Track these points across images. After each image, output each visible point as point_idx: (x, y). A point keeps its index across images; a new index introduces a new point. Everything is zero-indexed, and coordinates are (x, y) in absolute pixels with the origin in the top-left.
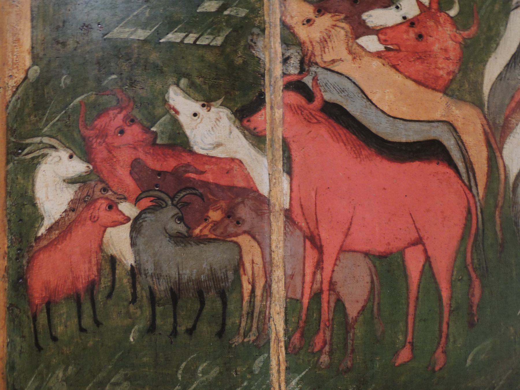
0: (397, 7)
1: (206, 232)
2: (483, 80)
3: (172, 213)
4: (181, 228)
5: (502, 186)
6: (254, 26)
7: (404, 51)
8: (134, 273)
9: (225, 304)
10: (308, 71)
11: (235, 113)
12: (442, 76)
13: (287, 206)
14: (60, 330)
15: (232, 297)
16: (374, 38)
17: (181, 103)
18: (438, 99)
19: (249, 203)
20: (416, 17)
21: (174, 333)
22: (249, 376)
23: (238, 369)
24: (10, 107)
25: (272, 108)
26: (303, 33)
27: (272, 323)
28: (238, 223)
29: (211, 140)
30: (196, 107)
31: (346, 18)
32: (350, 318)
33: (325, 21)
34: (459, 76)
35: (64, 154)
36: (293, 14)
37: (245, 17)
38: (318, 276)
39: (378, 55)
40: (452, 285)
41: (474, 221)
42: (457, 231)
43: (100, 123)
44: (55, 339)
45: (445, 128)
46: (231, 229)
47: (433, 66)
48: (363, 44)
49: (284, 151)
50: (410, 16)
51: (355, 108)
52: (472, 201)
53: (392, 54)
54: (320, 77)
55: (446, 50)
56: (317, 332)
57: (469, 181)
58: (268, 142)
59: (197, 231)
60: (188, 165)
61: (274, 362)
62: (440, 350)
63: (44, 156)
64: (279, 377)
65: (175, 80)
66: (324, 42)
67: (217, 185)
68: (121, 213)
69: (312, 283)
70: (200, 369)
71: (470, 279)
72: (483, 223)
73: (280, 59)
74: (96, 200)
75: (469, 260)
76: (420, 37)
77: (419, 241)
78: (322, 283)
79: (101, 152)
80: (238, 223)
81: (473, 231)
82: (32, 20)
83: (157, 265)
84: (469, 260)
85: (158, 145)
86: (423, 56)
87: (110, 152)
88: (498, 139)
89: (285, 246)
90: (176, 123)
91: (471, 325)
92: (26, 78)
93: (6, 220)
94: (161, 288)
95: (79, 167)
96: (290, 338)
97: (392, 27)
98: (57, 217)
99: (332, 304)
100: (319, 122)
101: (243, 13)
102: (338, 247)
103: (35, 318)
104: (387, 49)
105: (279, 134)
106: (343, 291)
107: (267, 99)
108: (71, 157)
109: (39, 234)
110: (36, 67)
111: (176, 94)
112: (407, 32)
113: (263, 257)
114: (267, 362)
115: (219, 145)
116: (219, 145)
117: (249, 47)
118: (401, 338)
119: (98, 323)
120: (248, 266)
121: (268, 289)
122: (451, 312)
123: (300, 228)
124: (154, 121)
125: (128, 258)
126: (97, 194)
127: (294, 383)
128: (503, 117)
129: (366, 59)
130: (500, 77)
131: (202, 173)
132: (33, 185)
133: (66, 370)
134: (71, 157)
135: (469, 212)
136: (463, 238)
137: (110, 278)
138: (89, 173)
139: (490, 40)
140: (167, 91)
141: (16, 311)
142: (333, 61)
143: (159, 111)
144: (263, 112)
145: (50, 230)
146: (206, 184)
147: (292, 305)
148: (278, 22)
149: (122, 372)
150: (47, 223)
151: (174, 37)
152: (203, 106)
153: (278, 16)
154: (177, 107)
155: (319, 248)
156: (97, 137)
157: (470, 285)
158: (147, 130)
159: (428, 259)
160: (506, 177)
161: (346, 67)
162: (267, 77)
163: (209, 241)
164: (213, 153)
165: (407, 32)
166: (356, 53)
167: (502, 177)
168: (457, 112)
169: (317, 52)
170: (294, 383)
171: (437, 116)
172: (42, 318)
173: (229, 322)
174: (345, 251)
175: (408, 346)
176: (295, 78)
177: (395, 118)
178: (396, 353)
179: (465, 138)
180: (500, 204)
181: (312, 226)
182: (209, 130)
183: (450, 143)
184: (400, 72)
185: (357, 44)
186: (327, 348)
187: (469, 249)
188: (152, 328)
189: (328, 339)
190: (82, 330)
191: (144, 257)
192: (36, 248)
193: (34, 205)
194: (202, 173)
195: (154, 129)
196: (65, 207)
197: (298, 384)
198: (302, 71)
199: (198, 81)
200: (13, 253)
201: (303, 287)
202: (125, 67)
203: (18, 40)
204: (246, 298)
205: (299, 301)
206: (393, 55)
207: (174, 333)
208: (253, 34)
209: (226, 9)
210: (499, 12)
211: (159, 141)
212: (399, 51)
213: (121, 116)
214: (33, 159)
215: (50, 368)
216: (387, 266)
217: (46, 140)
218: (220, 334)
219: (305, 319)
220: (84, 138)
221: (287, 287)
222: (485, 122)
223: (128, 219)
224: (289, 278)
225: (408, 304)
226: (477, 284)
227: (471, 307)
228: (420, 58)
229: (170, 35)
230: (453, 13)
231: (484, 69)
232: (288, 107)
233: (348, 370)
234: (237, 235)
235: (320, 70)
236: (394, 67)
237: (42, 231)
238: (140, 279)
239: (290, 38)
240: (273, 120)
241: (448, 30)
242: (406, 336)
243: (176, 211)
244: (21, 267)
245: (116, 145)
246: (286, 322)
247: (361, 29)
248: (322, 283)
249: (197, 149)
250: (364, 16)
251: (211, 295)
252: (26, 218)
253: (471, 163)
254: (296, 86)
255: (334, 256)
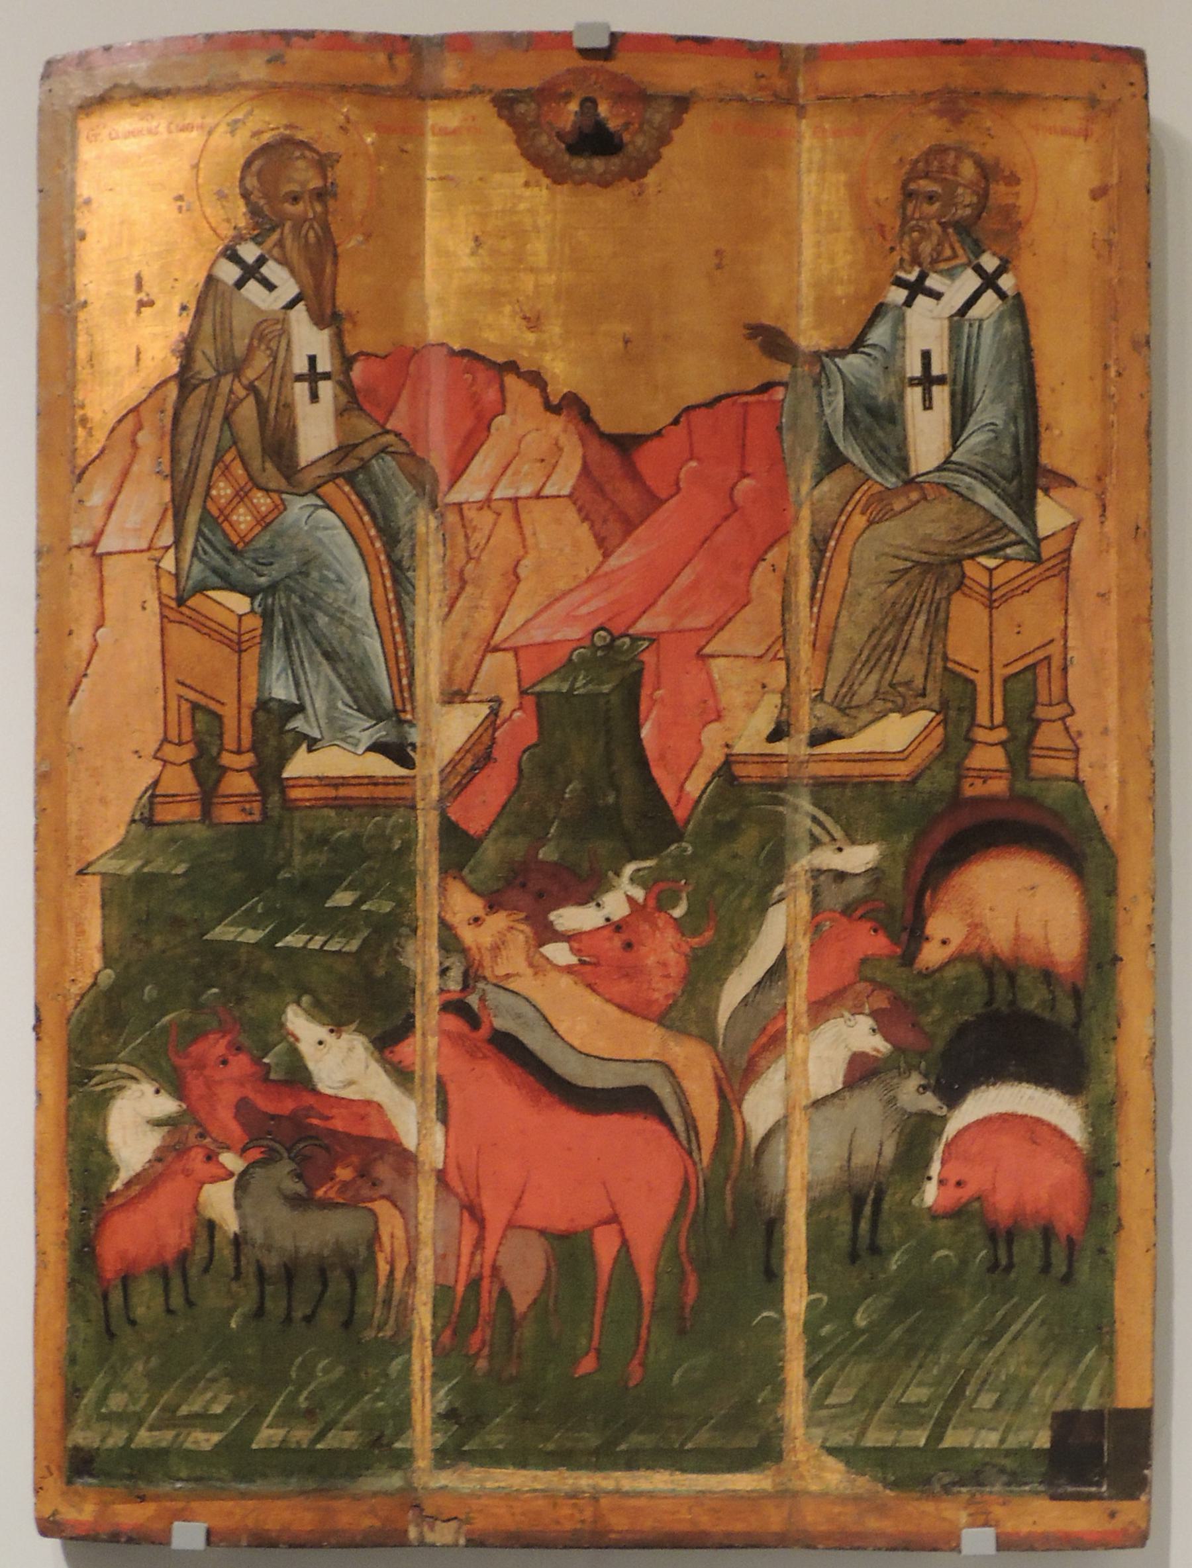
0: (598, 905)
1: (332, 1194)
2: (717, 1006)
3: (288, 1169)
4: (300, 1188)
5: (738, 1151)
6: (403, 925)
7: (606, 966)
8: (238, 1242)
9: (354, 1287)
10: (474, 988)
11: (373, 1042)
12: (657, 1000)
13: (440, 1166)
14: (140, 1312)
15: (364, 1281)
16: (564, 946)
17: (303, 1027)
18: (649, 1032)
19: (390, 1159)
20: (624, 919)
21: (288, 1319)
22: (383, 1381)
23: (370, 1370)
24: (73, 1020)
25: (424, 1035)
26: (468, 935)
27: (415, 1316)
28: (374, 1184)
29: (340, 1076)
30: (322, 1032)
31: (527, 918)
32: (517, 1312)
33: (498, 921)
34: (682, 1000)
35: (148, 1088)
36: (457, 909)
37: (390, 914)
38: (478, 1258)
39: (569, 969)
40: (657, 1279)
41: (693, 1197)
42: (668, 1208)
43: (195, 1050)
44: (133, 1323)
45: (658, 1070)
46: (366, 1192)
47: (645, 986)
48: (548, 955)
49: (438, 1092)
50: (616, 918)
51: (535, 1040)
52: (691, 1170)
53: (588, 968)
54: (489, 996)
55: (664, 964)
56: (474, 1330)
57: (689, 1142)
58: (417, 1080)
59: (320, 1193)
60: (311, 1107)
61: (416, 1367)
62: (636, 1362)
63: (121, 1088)
64: (423, 1386)
65: (294, 996)
66: (496, 949)
67: (348, 1135)
68: (223, 1167)
69: (470, 1266)
70: (320, 1366)
71: (683, 1273)
72: (707, 1198)
73: (436, 969)
74: (190, 1149)
75: (682, 1248)
76: (628, 946)
77: (614, 1219)
78: (482, 1266)
79: (196, 1086)
80: (374, 1184)
81: (692, 1209)
82: (103, 907)
83: (267, 1232)
84: (682, 1248)
85: (273, 1081)
86: (631, 972)
87: (209, 1088)
88: (736, 1087)
89: (436, 1218)
90: (294, 1053)
91: (682, 1332)
92: (95, 984)
93: (67, 1169)
94: (272, 1262)
95: (167, 1105)
96: (438, 1337)
97: (590, 932)
98: (138, 1168)
99: (495, 1295)
100: (485, 1057)
101: (387, 907)
102: (505, 1222)
103: (105, 1297)
104: (582, 963)
105: (433, 1070)
106: (509, 1279)
107: (418, 1024)
108: (157, 1092)
109: (114, 1189)
110: (109, 971)
111: (296, 1015)
112: (610, 939)
113: (407, 1231)
114: (408, 1365)
115: (351, 1083)
116: (351, 1083)
117: (395, 953)
118: (584, 1341)
119: (190, 1303)
120: (385, 1239)
121: (411, 1270)
122: (653, 1313)
123: (457, 1195)
124: (266, 1049)
125: (231, 1223)
126: (192, 1140)
127: (442, 1393)
128: (746, 1057)
129: (554, 974)
130: (745, 1001)
131: (328, 1118)
132: (105, 1125)
133: (147, 1362)
134: (157, 1092)
135: (686, 1184)
136: (676, 1218)
137: (207, 1248)
138: (182, 1114)
139: (731, 951)
140: (284, 1012)
141: (80, 1288)
142: (508, 976)
143: (273, 1037)
144: (411, 1040)
145: (128, 1185)
146: (333, 1133)
147: (442, 1294)
148: (436, 919)
149: (221, 1366)
150: (124, 1176)
151: (293, 940)
152: (332, 1031)
153: (436, 911)
154: (298, 1032)
155: (480, 1222)
156: (193, 1068)
157: (682, 1279)
158: (257, 1061)
159: (625, 1243)
160: (746, 1140)
161: (525, 984)
162: (418, 994)
163: (337, 1205)
164: (344, 1093)
165: (610, 939)
166: (539, 966)
167: (740, 1139)
168: (677, 1049)
169: (487, 962)
170: (442, 1393)
171: (648, 1053)
172: (116, 1298)
173: (359, 1310)
174: (514, 1227)
175: (592, 1354)
176: (455, 996)
177: (588, 1055)
178: (576, 1362)
179: (686, 1084)
180: (734, 1175)
181: (472, 1192)
182: (339, 1062)
183: (663, 1091)
184: (598, 994)
185: (543, 956)
186: (486, 1351)
187: (684, 1233)
188: (259, 1312)
189: (488, 1338)
190: (169, 1311)
191: (251, 1222)
192: (107, 1208)
193: (106, 1152)
194: (328, 1118)
195: (266, 1060)
196: (149, 1156)
197: (447, 1395)
198: (466, 987)
199: (326, 999)
200: (77, 1212)
201: (457, 1272)
202: (229, 977)
203: (83, 932)
204: (383, 1280)
205: (452, 1289)
206: (590, 970)
207: (288, 1319)
208: (400, 936)
209: (364, 902)
210: (750, 909)
211: (273, 1076)
212: (596, 965)
213: (223, 1042)
214: (104, 1091)
215: (127, 1361)
216: (568, 1249)
217: (123, 1068)
218: (347, 1324)
219: (459, 1313)
220: (175, 1069)
221: (437, 1270)
222: (717, 1064)
223: (231, 1174)
224: (441, 1258)
225: (595, 1299)
226: (692, 1279)
227: (683, 1308)
228: (627, 975)
229: (289, 938)
230: (678, 912)
231: (721, 990)
232: (445, 1034)
233: (512, 1380)
234: (372, 1200)
235: (489, 988)
236: (589, 986)
237: (117, 1186)
238: (246, 1249)
239: (450, 942)
240: (425, 1050)
241: (671, 936)
242: (591, 1339)
243: (293, 1166)
244: (86, 1231)
245: (217, 1078)
246: (435, 1315)
247: (546, 933)
248: (482, 1266)
249: (323, 1087)
250: (552, 916)
251: (336, 1275)
252: (94, 1169)
253: (694, 1119)
254: (456, 1007)
255: (500, 1233)
